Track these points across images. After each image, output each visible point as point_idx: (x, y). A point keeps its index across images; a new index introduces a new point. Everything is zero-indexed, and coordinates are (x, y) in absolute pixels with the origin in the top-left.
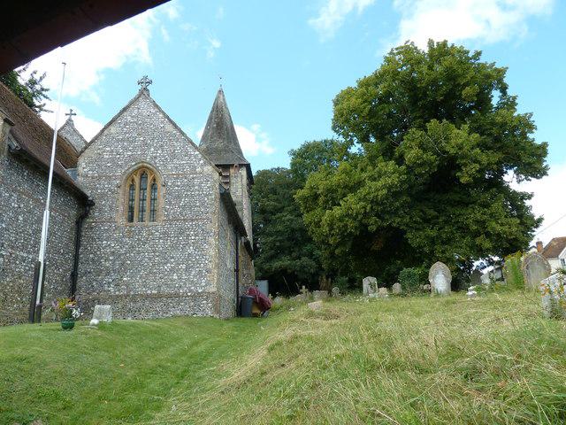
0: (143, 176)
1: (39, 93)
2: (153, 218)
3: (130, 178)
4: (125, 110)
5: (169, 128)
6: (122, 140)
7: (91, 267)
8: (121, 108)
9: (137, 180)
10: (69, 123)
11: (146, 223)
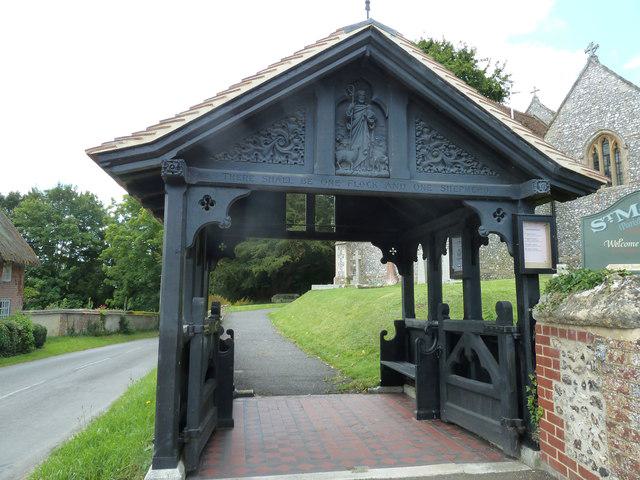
0: (604, 142)
1: (505, 79)
2: (620, 182)
3: (592, 147)
4: (576, 84)
5: (624, 88)
6: (579, 114)
7: (568, 233)
8: (572, 84)
9: (599, 148)
10: (535, 100)
11: (614, 187)
